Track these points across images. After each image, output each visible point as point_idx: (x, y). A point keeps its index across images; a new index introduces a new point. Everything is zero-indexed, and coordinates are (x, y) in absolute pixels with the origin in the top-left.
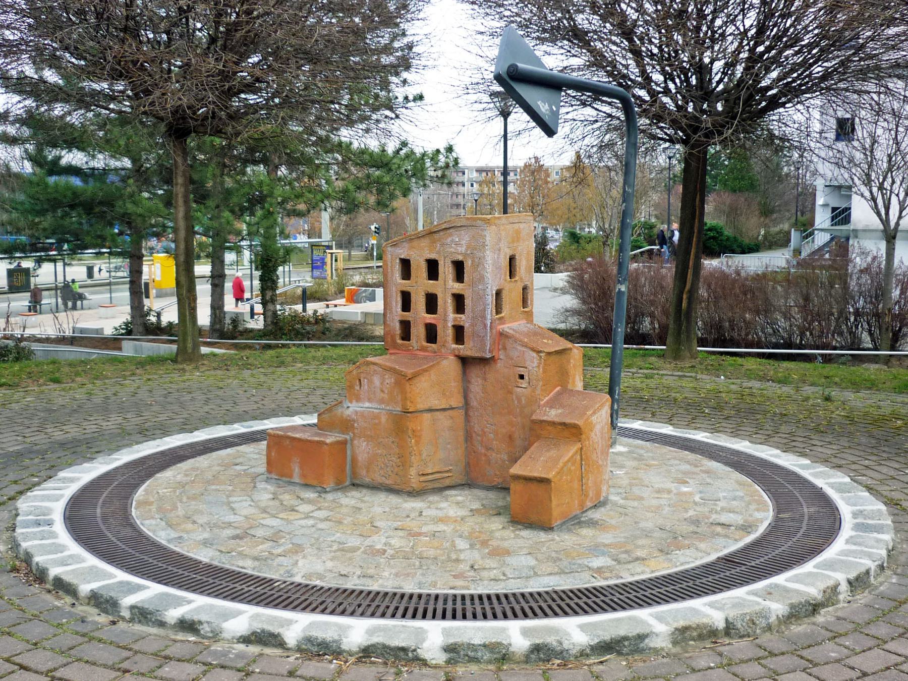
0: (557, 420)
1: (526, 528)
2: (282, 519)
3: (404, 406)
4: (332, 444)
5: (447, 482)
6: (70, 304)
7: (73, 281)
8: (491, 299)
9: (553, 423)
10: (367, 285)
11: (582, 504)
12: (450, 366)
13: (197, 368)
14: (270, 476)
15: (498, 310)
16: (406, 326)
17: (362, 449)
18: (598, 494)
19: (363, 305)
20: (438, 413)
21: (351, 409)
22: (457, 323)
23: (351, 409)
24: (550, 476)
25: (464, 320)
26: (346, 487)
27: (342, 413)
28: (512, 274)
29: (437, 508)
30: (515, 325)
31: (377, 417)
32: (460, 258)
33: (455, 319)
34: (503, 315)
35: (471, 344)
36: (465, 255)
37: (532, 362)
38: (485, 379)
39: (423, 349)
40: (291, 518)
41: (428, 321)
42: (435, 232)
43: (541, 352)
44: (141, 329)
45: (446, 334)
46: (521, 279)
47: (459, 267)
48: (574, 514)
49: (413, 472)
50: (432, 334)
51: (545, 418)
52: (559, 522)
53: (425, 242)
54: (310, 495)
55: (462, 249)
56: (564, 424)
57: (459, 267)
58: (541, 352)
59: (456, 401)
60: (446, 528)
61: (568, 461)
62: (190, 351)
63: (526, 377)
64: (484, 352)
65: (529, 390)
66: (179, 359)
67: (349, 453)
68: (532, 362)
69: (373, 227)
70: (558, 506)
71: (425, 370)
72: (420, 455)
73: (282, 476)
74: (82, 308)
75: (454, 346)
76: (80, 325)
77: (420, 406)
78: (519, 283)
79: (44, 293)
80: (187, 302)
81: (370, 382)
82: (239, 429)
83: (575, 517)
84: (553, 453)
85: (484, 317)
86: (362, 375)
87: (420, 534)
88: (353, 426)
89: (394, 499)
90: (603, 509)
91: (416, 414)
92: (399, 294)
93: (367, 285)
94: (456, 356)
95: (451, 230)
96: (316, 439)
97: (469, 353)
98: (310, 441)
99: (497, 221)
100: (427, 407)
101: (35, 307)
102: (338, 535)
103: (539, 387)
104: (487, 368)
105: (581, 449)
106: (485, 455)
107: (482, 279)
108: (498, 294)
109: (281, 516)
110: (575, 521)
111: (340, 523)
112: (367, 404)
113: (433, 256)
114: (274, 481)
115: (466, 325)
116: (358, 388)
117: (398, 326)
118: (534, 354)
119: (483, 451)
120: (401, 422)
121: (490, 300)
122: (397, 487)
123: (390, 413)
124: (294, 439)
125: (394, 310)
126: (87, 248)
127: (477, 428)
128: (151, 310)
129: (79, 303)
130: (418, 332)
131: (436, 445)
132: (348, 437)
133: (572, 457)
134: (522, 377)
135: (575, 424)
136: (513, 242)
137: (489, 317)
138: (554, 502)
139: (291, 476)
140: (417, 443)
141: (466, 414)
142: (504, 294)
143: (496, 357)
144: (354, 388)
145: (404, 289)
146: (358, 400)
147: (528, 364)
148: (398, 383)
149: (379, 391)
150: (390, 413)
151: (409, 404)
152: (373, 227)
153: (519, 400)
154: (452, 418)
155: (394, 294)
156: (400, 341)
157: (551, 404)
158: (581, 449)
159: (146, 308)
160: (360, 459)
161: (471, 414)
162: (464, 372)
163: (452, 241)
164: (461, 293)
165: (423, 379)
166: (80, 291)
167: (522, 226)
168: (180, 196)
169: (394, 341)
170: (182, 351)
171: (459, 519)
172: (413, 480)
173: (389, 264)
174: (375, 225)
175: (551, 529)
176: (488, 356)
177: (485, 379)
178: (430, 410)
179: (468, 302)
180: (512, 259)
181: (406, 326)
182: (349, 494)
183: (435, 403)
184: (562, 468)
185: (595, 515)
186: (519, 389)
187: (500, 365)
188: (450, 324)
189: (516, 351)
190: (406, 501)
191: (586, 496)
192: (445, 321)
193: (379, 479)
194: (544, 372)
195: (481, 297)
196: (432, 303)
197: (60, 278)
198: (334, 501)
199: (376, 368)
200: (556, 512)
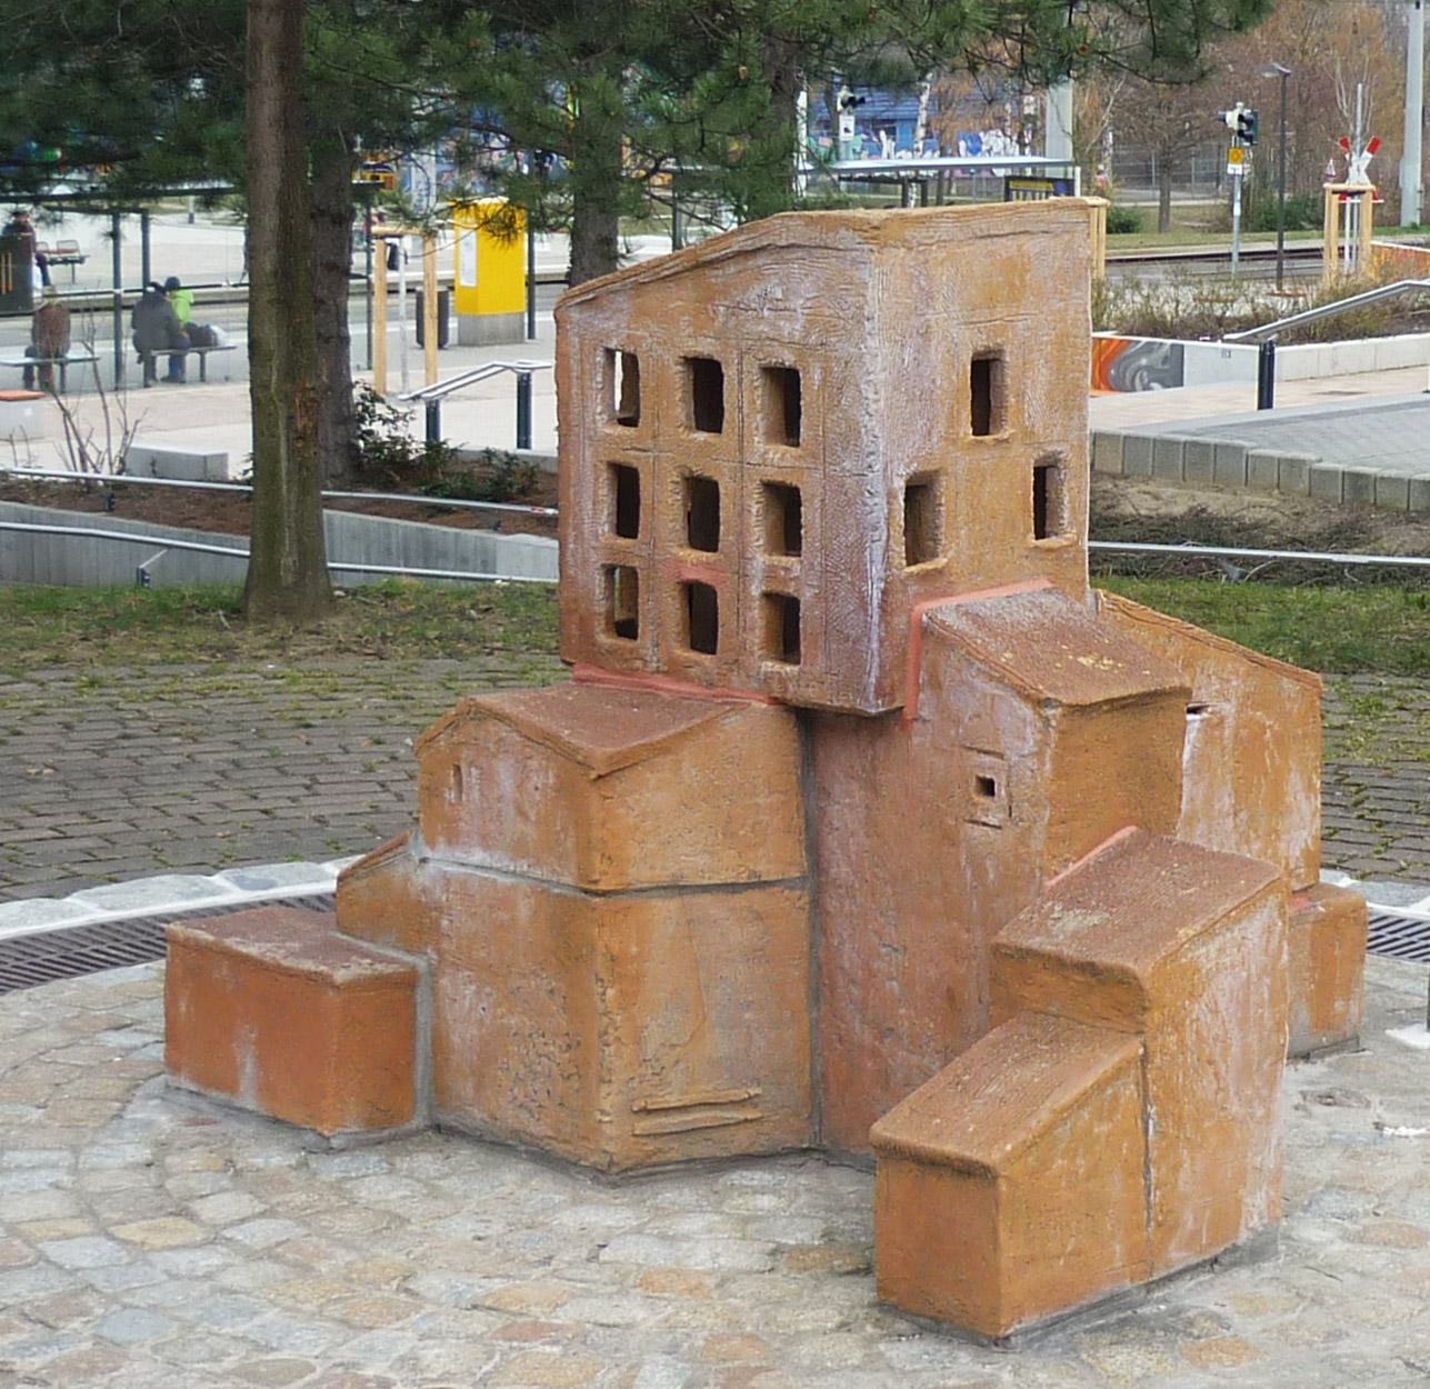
0: (1070, 952)
1: (922, 1330)
2: (125, 1242)
3: (583, 873)
4: (352, 986)
5: (741, 1141)
6: (162, 362)
7: (173, 284)
8: (884, 510)
9: (1057, 963)
10: (1156, 327)
11: (1143, 1257)
12: (751, 738)
13: (281, 645)
14: (173, 1081)
15: (918, 548)
16: (625, 581)
17: (463, 1008)
18: (1226, 1215)
19: (1139, 396)
20: (705, 899)
21: (435, 866)
22: (776, 587)
23: (431, 866)
24: (993, 1157)
25: (798, 575)
26: (409, 1135)
27: (407, 879)
28: (983, 420)
29: (663, 1237)
30: (987, 600)
31: (505, 901)
32: (788, 359)
33: (771, 571)
34: (940, 562)
35: (821, 663)
36: (803, 348)
37: (1022, 741)
38: (873, 788)
39: (675, 670)
40: (157, 1240)
41: (691, 575)
42: (711, 263)
43: (1047, 703)
44: (338, 465)
45: (745, 623)
46: (1029, 434)
47: (785, 383)
48: (1107, 1289)
49: (609, 1100)
50: (701, 615)
51: (1035, 942)
52: (1031, 1320)
53: (679, 299)
54: (274, 1157)
55: (793, 328)
56: (1089, 968)
57: (785, 383)
58: (1047, 703)
59: (777, 857)
60: (640, 1314)
61: (1081, 1102)
62: (289, 579)
63: (1001, 790)
64: (861, 692)
65: (1011, 833)
66: (253, 608)
67: (423, 1017)
68: (1022, 741)
69: (1232, 118)
70: (1022, 1260)
71: (662, 749)
72: (638, 1041)
73: (209, 1085)
74: (203, 379)
75: (770, 666)
76: (146, 442)
77: (640, 874)
78: (1017, 449)
79: (76, 321)
80: (282, 413)
81: (488, 778)
82: (85, 909)
83: (1113, 1301)
84: (1034, 1072)
85: (859, 571)
86: (465, 754)
87: (538, 1331)
88: (436, 924)
89: (541, 1191)
90: (1243, 1274)
91: (625, 900)
92: (605, 475)
93: (1156, 327)
94: (775, 701)
95: (760, 260)
96: (308, 965)
97: (812, 694)
98: (290, 973)
99: (919, 234)
100: (663, 875)
101: (45, 369)
102: (271, 1314)
103: (1039, 830)
104: (881, 745)
105: (1145, 1059)
106: (875, 1053)
107: (851, 436)
108: (919, 492)
109: (123, 1232)
110: (1111, 1314)
111: (305, 1269)
112: (478, 856)
113: (705, 347)
114: (184, 1099)
115: (806, 596)
116: (451, 796)
117: (598, 581)
118: (1026, 711)
119: (867, 1037)
120: (578, 923)
121: (880, 513)
122: (560, 1148)
123: (542, 890)
124: (246, 959)
125: (586, 528)
126: (182, 178)
127: (849, 957)
128: (375, 398)
129: (192, 359)
130: (662, 611)
131: (695, 1008)
132: (421, 964)
133: (1100, 1086)
134: (988, 787)
135: (1124, 971)
136: (991, 301)
137: (876, 570)
138: (1011, 1247)
139: (232, 1088)
140: (627, 999)
141: (816, 905)
142: (947, 494)
143: (908, 713)
144: (440, 795)
145: (619, 457)
146: (453, 839)
147: (1007, 742)
148: (566, 790)
149: (510, 811)
150: (542, 890)
151: (599, 865)
152: (1232, 118)
153: (979, 872)
154: (759, 917)
155: (589, 476)
156: (605, 639)
157: (1073, 896)
158: (1145, 1059)
159: (357, 393)
160: (455, 1039)
161: (832, 905)
162: (809, 760)
163: (764, 296)
164: (791, 480)
165: (652, 779)
166: (197, 317)
167: (1031, 245)
168: (265, 48)
169: (587, 636)
170: (263, 572)
171: (711, 1282)
172: (608, 1130)
173: (575, 367)
174: (1240, 109)
175: (1001, 1342)
176: (874, 707)
177: (873, 788)
178: (677, 889)
179: (809, 514)
180: (984, 371)
181: (625, 581)
182: (403, 1164)
183: (695, 863)
184: (1050, 1128)
185: (1201, 1297)
186: (978, 831)
187: (919, 739)
188: (756, 590)
189: (974, 694)
190: (576, 1202)
191: (1167, 1227)
192: (743, 576)
193: (512, 1117)
194: (1059, 773)
195: (847, 500)
196: (703, 501)
197: (131, 276)
198: (337, 1187)
199: (503, 730)
200: (1014, 1288)
